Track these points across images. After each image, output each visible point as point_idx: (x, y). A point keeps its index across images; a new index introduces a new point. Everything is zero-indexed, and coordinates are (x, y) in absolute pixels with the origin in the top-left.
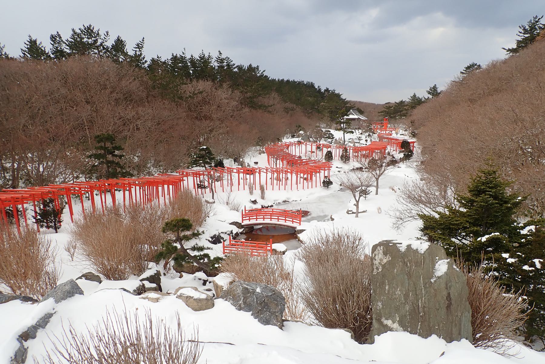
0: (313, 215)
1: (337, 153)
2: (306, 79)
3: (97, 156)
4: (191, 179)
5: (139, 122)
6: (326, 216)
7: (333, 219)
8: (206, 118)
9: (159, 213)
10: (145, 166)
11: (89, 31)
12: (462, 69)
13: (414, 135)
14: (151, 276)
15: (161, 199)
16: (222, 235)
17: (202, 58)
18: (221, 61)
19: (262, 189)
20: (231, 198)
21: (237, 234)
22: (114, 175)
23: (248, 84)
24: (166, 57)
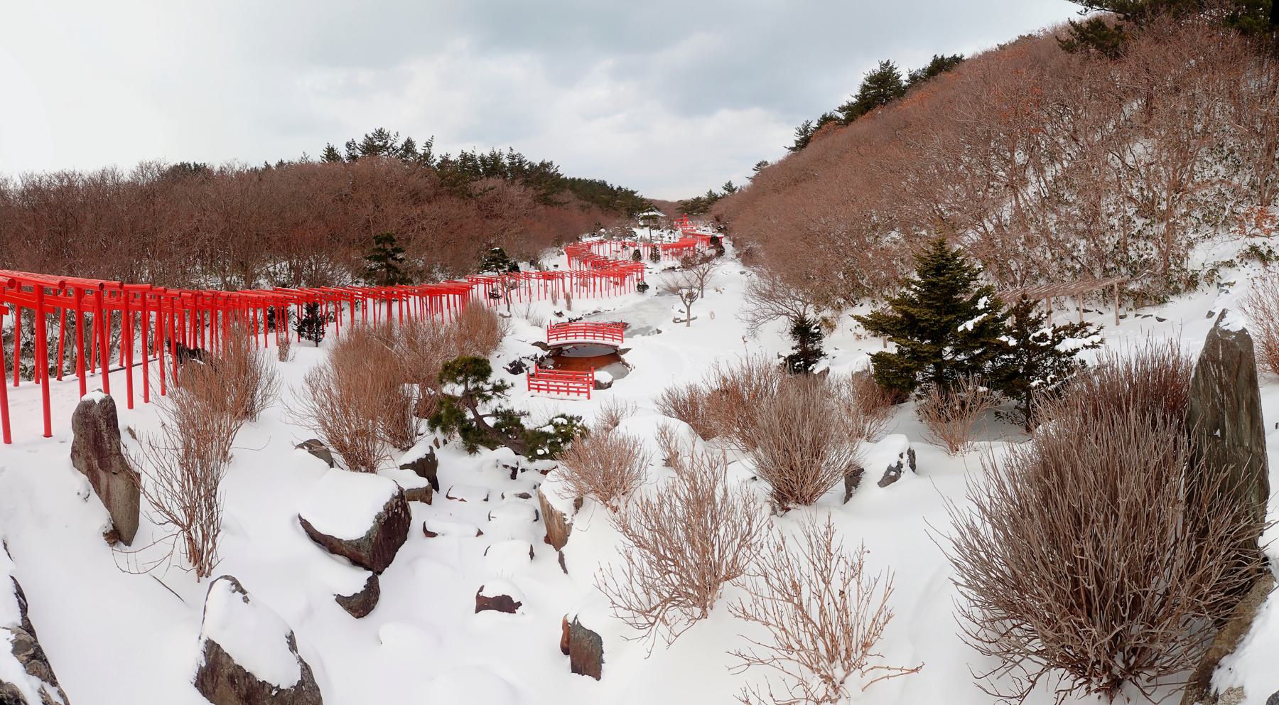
0: (634, 327)
1: (646, 252)
2: (597, 177)
3: (378, 259)
4: (481, 286)
5: (424, 222)
6: (649, 328)
7: (659, 332)
8: (496, 216)
9: (442, 332)
10: (430, 271)
11: (380, 134)
12: (754, 166)
13: (720, 230)
14: (420, 460)
15: (446, 311)
16: (524, 361)
17: (493, 155)
18: (513, 157)
19: (568, 298)
20: (532, 310)
21: (542, 359)
22: (391, 283)
23: (542, 182)
24: (455, 156)
